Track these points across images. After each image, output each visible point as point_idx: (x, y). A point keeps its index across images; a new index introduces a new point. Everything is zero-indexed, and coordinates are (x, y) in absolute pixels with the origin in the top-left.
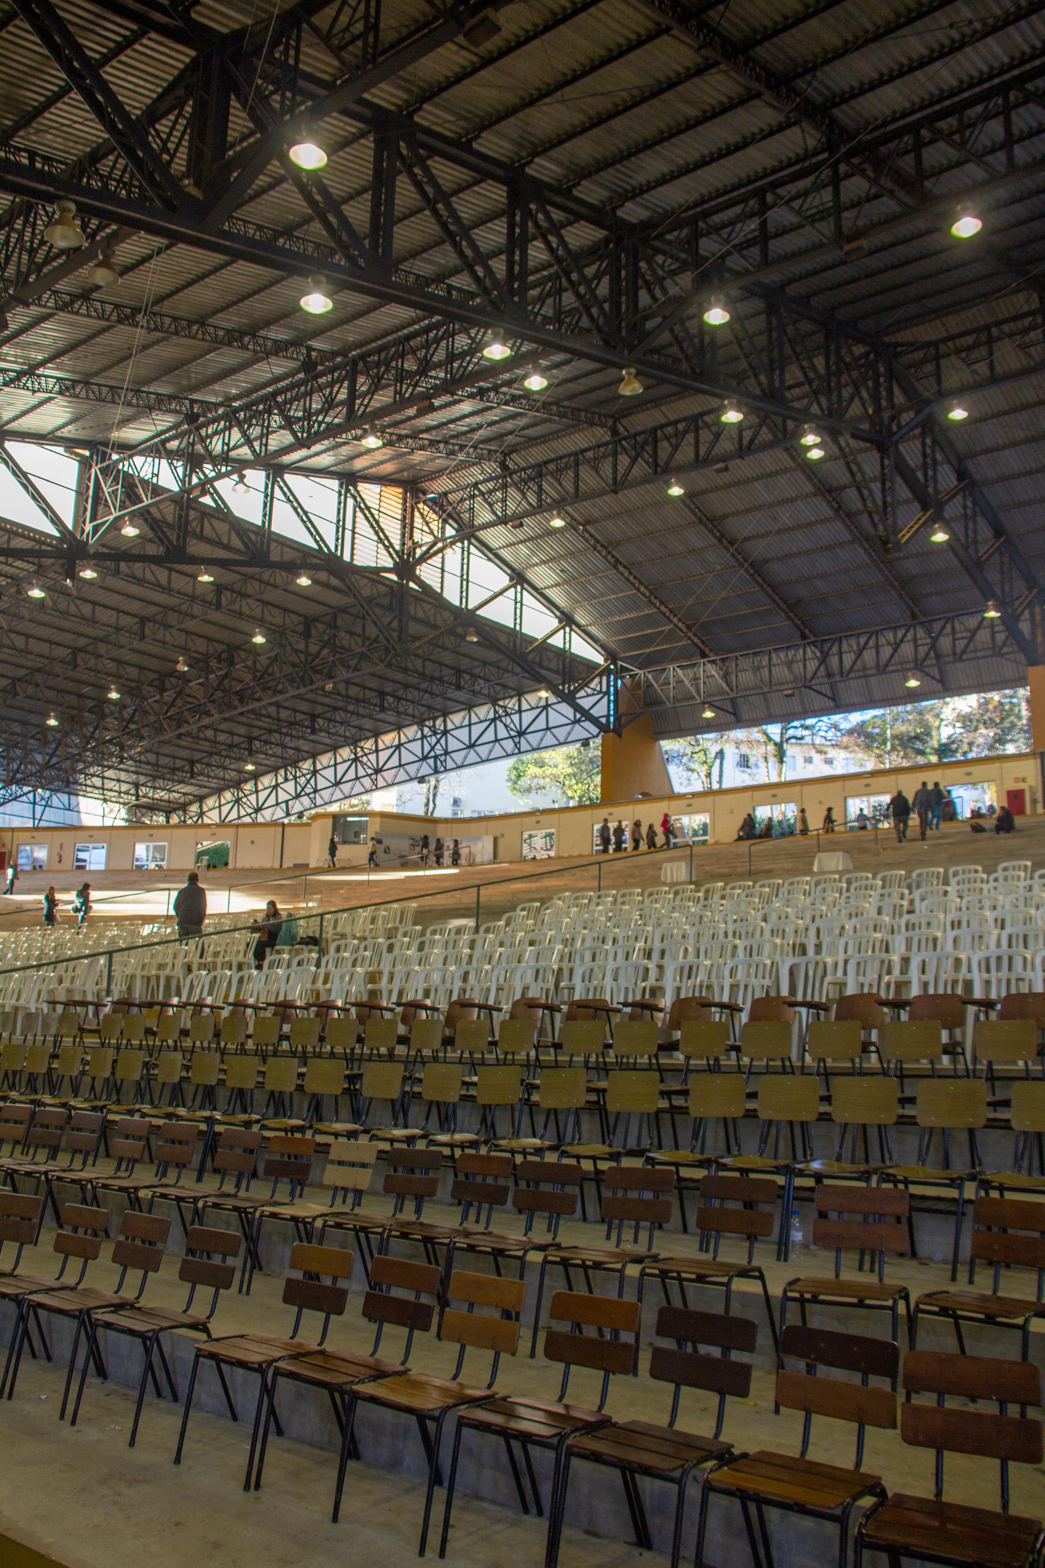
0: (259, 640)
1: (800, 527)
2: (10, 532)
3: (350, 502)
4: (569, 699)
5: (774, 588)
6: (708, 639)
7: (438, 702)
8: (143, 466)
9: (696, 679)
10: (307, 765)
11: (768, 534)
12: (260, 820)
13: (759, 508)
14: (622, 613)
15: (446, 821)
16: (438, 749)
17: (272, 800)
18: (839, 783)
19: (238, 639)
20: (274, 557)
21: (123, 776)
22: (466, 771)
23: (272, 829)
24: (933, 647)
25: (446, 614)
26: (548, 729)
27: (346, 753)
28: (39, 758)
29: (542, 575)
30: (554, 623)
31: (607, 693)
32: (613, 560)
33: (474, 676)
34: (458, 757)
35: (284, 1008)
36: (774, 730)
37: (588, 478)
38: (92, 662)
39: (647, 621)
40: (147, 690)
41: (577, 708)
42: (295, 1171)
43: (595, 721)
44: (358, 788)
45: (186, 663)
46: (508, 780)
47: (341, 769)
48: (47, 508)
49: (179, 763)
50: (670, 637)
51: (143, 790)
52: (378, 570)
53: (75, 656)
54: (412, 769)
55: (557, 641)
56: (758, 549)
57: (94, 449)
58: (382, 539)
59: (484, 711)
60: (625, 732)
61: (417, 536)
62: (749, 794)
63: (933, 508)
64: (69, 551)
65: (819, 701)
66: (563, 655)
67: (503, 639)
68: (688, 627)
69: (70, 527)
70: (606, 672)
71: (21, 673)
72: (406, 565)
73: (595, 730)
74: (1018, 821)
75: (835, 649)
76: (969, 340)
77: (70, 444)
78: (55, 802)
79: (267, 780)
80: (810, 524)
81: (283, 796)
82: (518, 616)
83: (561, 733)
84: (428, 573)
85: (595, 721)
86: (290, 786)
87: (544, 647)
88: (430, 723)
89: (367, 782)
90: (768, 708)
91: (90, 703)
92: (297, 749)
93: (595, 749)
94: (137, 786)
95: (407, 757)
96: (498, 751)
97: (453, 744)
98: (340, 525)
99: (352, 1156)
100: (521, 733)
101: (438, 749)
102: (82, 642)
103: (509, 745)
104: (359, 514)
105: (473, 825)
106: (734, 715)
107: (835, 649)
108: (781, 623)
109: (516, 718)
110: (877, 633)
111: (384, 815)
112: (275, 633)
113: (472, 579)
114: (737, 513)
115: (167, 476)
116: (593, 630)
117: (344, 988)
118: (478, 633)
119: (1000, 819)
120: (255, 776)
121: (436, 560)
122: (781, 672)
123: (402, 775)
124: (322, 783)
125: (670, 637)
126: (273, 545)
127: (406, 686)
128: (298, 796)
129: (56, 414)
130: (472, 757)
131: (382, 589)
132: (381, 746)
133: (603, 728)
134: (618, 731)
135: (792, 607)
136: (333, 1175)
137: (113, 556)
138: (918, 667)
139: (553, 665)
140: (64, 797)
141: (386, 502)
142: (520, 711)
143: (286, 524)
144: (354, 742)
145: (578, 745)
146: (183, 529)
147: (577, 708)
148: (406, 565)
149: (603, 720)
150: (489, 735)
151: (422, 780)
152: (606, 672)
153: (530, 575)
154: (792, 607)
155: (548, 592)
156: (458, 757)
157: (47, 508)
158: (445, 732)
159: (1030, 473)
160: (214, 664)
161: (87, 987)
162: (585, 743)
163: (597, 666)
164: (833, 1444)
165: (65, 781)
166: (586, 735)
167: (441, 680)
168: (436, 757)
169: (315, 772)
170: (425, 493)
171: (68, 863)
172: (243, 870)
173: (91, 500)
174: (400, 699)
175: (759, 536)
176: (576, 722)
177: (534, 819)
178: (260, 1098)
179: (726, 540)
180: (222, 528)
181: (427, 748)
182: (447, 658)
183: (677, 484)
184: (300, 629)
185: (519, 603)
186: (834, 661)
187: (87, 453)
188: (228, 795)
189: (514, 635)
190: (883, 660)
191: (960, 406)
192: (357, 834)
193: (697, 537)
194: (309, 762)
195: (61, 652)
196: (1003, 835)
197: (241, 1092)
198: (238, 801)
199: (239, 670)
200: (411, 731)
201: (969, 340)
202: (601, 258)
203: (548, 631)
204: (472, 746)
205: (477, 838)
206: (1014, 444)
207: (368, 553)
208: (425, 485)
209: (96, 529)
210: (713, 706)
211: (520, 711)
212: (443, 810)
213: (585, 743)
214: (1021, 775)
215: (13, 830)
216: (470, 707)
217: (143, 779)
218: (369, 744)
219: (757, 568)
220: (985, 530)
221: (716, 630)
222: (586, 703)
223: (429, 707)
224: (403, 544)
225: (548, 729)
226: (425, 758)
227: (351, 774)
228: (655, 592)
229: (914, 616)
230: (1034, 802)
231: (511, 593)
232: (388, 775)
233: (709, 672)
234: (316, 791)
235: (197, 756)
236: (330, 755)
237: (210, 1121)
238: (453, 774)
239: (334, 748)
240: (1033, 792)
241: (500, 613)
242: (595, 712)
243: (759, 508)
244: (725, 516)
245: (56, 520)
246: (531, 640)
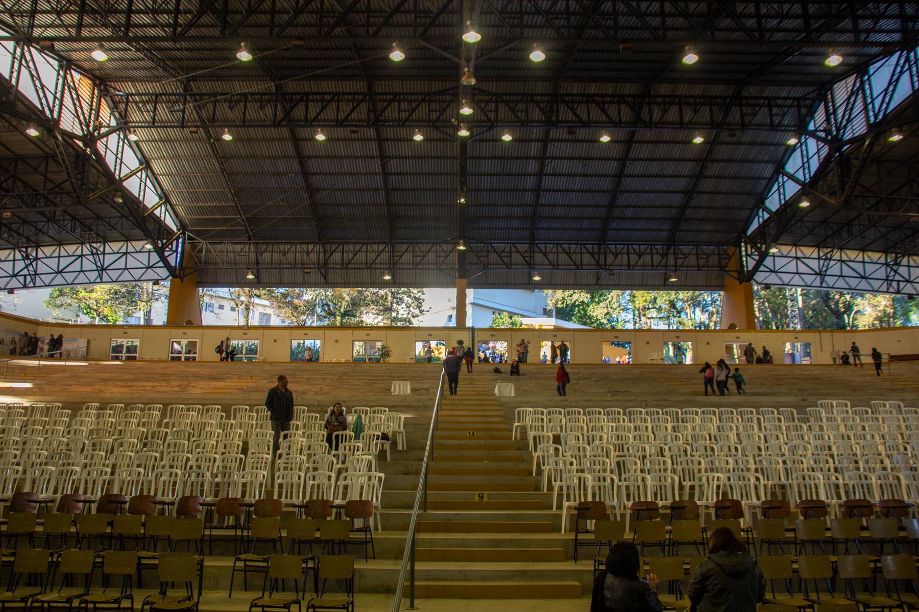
18: (571, 333)
26: (82, 271)
31: (177, 251)
34: (47, 279)
37: (253, 111)
52: (72, 136)
60: (185, 279)
62: (288, 331)
74: (522, 367)
90: (281, 277)
113: (120, 155)
116: (179, 209)
118: (122, 198)
119: (513, 366)
142: (104, 253)
143: (26, 87)
151: (11, 291)
155: (161, 178)
158: (36, 259)
183: (419, 132)
191: (699, 135)
196: (514, 377)
231: (125, 171)
238: (780, 334)
241: (132, 185)
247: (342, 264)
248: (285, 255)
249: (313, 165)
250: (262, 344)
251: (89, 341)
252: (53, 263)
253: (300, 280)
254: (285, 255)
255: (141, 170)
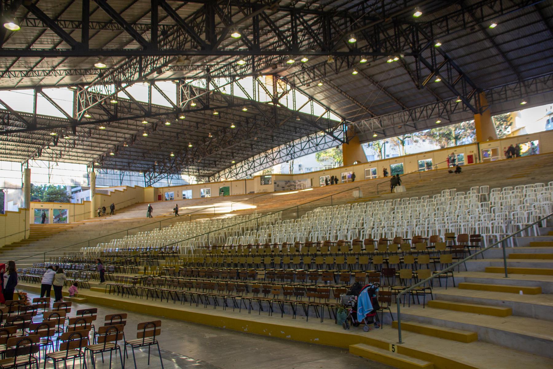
0: (233, 126)
1: (397, 76)
2: (159, 108)
3: (257, 82)
4: (331, 134)
5: (392, 95)
6: (374, 111)
7: (291, 137)
8: (195, 83)
9: (371, 124)
10: (251, 159)
11: (387, 79)
12: (238, 178)
13: (384, 72)
14: (345, 106)
15: (296, 175)
16: (292, 152)
17: (241, 171)
18: (416, 156)
19: (226, 125)
20: (235, 102)
21: (194, 167)
22: (301, 158)
23: (242, 182)
24: (445, 108)
25: (289, 113)
26: (325, 143)
27: (263, 154)
28: (168, 165)
29: (319, 97)
30: (324, 110)
31: (343, 130)
32: (340, 90)
33: (301, 129)
34: (298, 154)
35: (249, 246)
36: (401, 137)
38: (183, 136)
39: (354, 107)
40: (200, 142)
41: (334, 137)
42: (253, 276)
43: (339, 140)
44: (268, 166)
45: (212, 135)
46: (315, 159)
47: (262, 160)
48: (169, 100)
49: (211, 162)
50: (361, 111)
51: (201, 171)
52: (267, 103)
53: (177, 135)
54: (284, 158)
55: (325, 116)
56: (386, 84)
57: (181, 80)
58: (268, 93)
59: (305, 139)
60: (350, 142)
61: (278, 89)
62: (339, 169)
63: (436, 72)
64: (177, 111)
65: (410, 129)
66: (328, 120)
67: (308, 118)
68: (367, 108)
69: (176, 104)
70: (342, 124)
71: (162, 141)
72: (275, 100)
73: (340, 143)
75: (414, 111)
76: (441, 20)
77: (173, 80)
78: (174, 177)
79: (239, 165)
80: (401, 75)
81: (244, 170)
82: (312, 110)
83: (330, 144)
84: (283, 101)
85: (339, 140)
86: (246, 166)
87: (321, 118)
88: (289, 143)
89: (270, 163)
91: (183, 148)
92: (248, 155)
93: (341, 147)
94: (199, 170)
95: (282, 155)
96: (310, 151)
97: (296, 150)
98: (254, 90)
99: (261, 273)
100: (317, 145)
101: (292, 152)
102: (179, 131)
103: (314, 149)
104: (260, 86)
105: (304, 176)
106: (384, 134)
107: (414, 111)
108: (395, 104)
109: (315, 140)
110: (426, 106)
111: (276, 175)
112: (238, 124)
113: (296, 101)
114: (377, 74)
115: (200, 84)
116: (337, 111)
117: (263, 239)
120: (235, 164)
121: (285, 96)
122: (397, 120)
123: (281, 161)
124: (256, 165)
125: (361, 111)
126: (235, 100)
127: (280, 133)
128: (249, 169)
129: (168, 73)
130: (303, 153)
131: (268, 108)
132: (274, 152)
133: (343, 142)
134: (347, 143)
135: (398, 100)
136: (259, 277)
137: (188, 110)
138: (440, 116)
139: (325, 123)
140: (177, 175)
141: (267, 80)
142: (316, 138)
143: (238, 93)
144: (265, 151)
145: (335, 148)
146: (208, 100)
147: (334, 137)
148: (275, 100)
149: (342, 139)
150: (307, 146)
151: (287, 162)
152: (342, 124)
153: (315, 97)
154: (398, 100)
155: (321, 101)
156: (298, 154)
157: (169, 100)
158: (294, 146)
159: (468, 55)
160: (220, 133)
161: (203, 241)
162: (338, 147)
163: (339, 122)
164: (312, 300)
165: (176, 170)
166: (338, 144)
167: (290, 130)
168: (291, 154)
169: (254, 161)
170: (280, 76)
171: (181, 197)
172: (234, 196)
173: (181, 96)
174: (278, 137)
175: (385, 80)
176: (334, 140)
177: (323, 173)
178: (246, 265)
179: (375, 82)
180: (219, 97)
181: (288, 152)
182: (292, 124)
184: (245, 121)
185: (312, 106)
186: (414, 115)
187: (178, 81)
188: (227, 170)
189: (312, 117)
190: (429, 114)
192: (268, 181)
193: (365, 82)
194: (252, 158)
195: (157, 144)
196: (458, 174)
197: (257, 264)
198: (230, 172)
199: (228, 134)
200: (283, 146)
201: (441, 20)
202: (320, 22)
203: (322, 113)
204: (302, 150)
205: (305, 180)
206: (461, 47)
207: (264, 98)
208: (279, 74)
209: (183, 104)
210: (376, 132)
211: (316, 138)
212: (296, 171)
213: (338, 147)
214: (472, 150)
215: (163, 188)
216: (301, 138)
217: (200, 168)
218: (270, 151)
219: (386, 90)
220: (455, 73)
221: (373, 111)
222: (336, 134)
223: (288, 139)
224: (274, 93)
225: (325, 143)
226: (288, 155)
227: (265, 161)
228: (354, 99)
229: (438, 100)
230: (476, 158)
232: (277, 161)
233: (375, 122)
234: (255, 167)
235: (217, 159)
236: (258, 155)
237: (238, 270)
239: (259, 153)
240: (475, 156)
241: (306, 110)
242: (339, 137)
243: (384, 72)
244: (373, 75)
245: (172, 103)
246: (317, 117)
247: (427, 116)
248: (545, 84)
249: (499, 39)
250: (434, 160)
251: (311, 180)
252: (299, 146)
253: (404, 131)
254: (545, 84)
255: (447, 62)
